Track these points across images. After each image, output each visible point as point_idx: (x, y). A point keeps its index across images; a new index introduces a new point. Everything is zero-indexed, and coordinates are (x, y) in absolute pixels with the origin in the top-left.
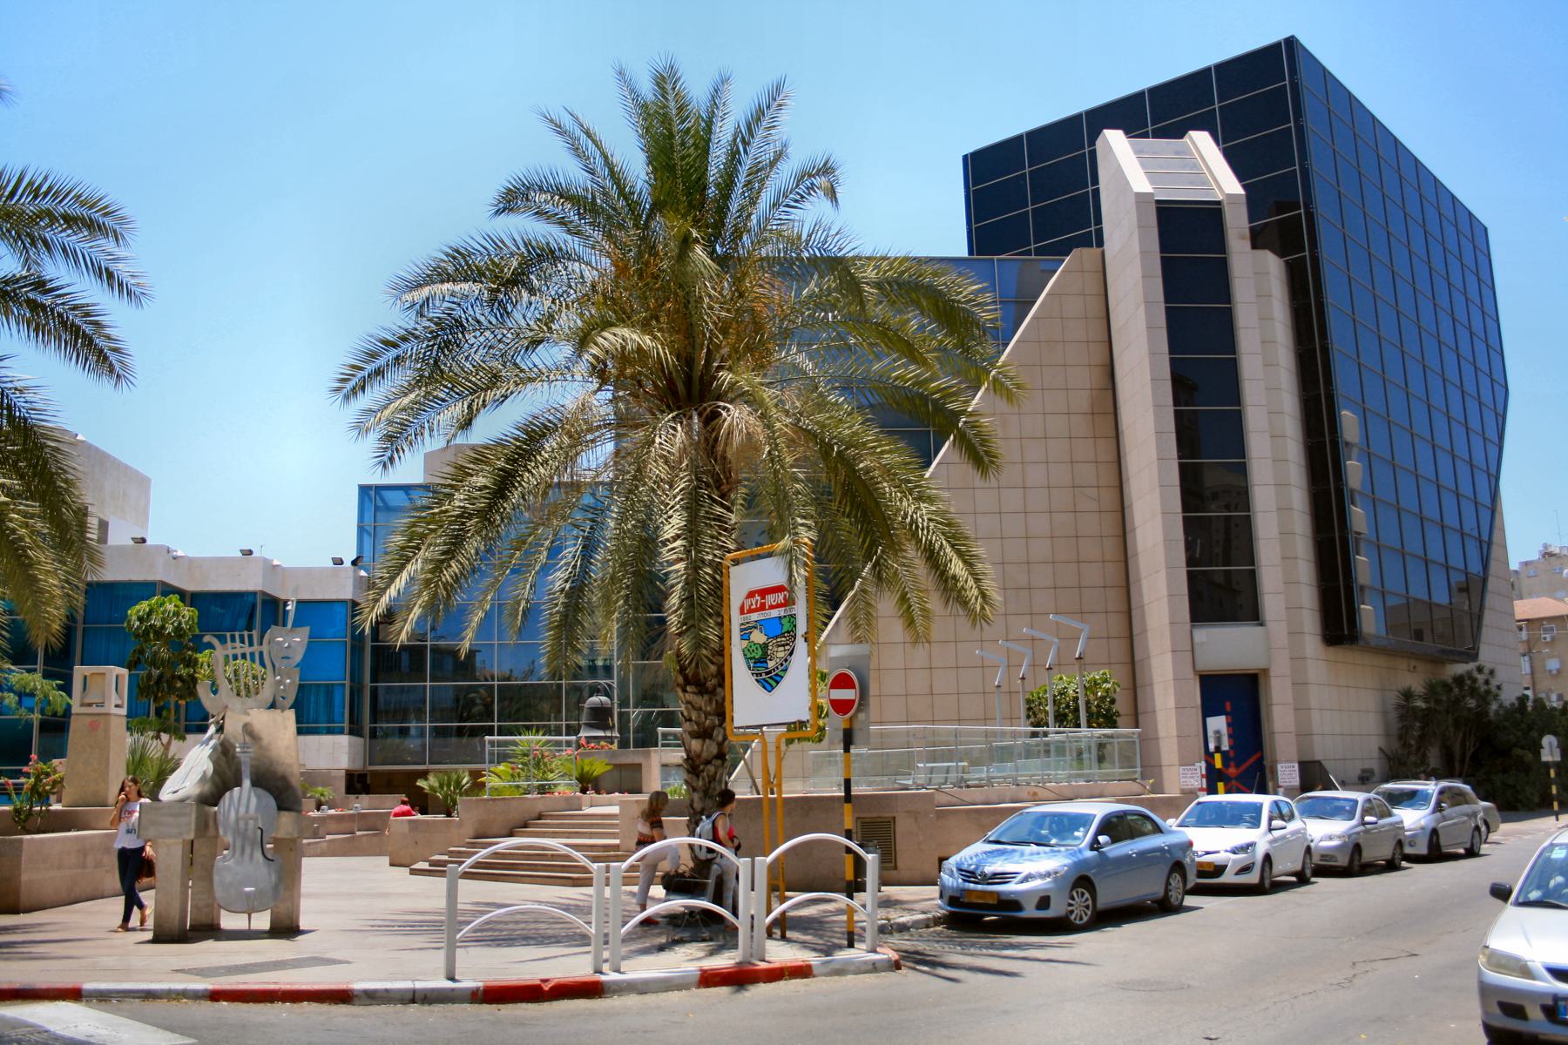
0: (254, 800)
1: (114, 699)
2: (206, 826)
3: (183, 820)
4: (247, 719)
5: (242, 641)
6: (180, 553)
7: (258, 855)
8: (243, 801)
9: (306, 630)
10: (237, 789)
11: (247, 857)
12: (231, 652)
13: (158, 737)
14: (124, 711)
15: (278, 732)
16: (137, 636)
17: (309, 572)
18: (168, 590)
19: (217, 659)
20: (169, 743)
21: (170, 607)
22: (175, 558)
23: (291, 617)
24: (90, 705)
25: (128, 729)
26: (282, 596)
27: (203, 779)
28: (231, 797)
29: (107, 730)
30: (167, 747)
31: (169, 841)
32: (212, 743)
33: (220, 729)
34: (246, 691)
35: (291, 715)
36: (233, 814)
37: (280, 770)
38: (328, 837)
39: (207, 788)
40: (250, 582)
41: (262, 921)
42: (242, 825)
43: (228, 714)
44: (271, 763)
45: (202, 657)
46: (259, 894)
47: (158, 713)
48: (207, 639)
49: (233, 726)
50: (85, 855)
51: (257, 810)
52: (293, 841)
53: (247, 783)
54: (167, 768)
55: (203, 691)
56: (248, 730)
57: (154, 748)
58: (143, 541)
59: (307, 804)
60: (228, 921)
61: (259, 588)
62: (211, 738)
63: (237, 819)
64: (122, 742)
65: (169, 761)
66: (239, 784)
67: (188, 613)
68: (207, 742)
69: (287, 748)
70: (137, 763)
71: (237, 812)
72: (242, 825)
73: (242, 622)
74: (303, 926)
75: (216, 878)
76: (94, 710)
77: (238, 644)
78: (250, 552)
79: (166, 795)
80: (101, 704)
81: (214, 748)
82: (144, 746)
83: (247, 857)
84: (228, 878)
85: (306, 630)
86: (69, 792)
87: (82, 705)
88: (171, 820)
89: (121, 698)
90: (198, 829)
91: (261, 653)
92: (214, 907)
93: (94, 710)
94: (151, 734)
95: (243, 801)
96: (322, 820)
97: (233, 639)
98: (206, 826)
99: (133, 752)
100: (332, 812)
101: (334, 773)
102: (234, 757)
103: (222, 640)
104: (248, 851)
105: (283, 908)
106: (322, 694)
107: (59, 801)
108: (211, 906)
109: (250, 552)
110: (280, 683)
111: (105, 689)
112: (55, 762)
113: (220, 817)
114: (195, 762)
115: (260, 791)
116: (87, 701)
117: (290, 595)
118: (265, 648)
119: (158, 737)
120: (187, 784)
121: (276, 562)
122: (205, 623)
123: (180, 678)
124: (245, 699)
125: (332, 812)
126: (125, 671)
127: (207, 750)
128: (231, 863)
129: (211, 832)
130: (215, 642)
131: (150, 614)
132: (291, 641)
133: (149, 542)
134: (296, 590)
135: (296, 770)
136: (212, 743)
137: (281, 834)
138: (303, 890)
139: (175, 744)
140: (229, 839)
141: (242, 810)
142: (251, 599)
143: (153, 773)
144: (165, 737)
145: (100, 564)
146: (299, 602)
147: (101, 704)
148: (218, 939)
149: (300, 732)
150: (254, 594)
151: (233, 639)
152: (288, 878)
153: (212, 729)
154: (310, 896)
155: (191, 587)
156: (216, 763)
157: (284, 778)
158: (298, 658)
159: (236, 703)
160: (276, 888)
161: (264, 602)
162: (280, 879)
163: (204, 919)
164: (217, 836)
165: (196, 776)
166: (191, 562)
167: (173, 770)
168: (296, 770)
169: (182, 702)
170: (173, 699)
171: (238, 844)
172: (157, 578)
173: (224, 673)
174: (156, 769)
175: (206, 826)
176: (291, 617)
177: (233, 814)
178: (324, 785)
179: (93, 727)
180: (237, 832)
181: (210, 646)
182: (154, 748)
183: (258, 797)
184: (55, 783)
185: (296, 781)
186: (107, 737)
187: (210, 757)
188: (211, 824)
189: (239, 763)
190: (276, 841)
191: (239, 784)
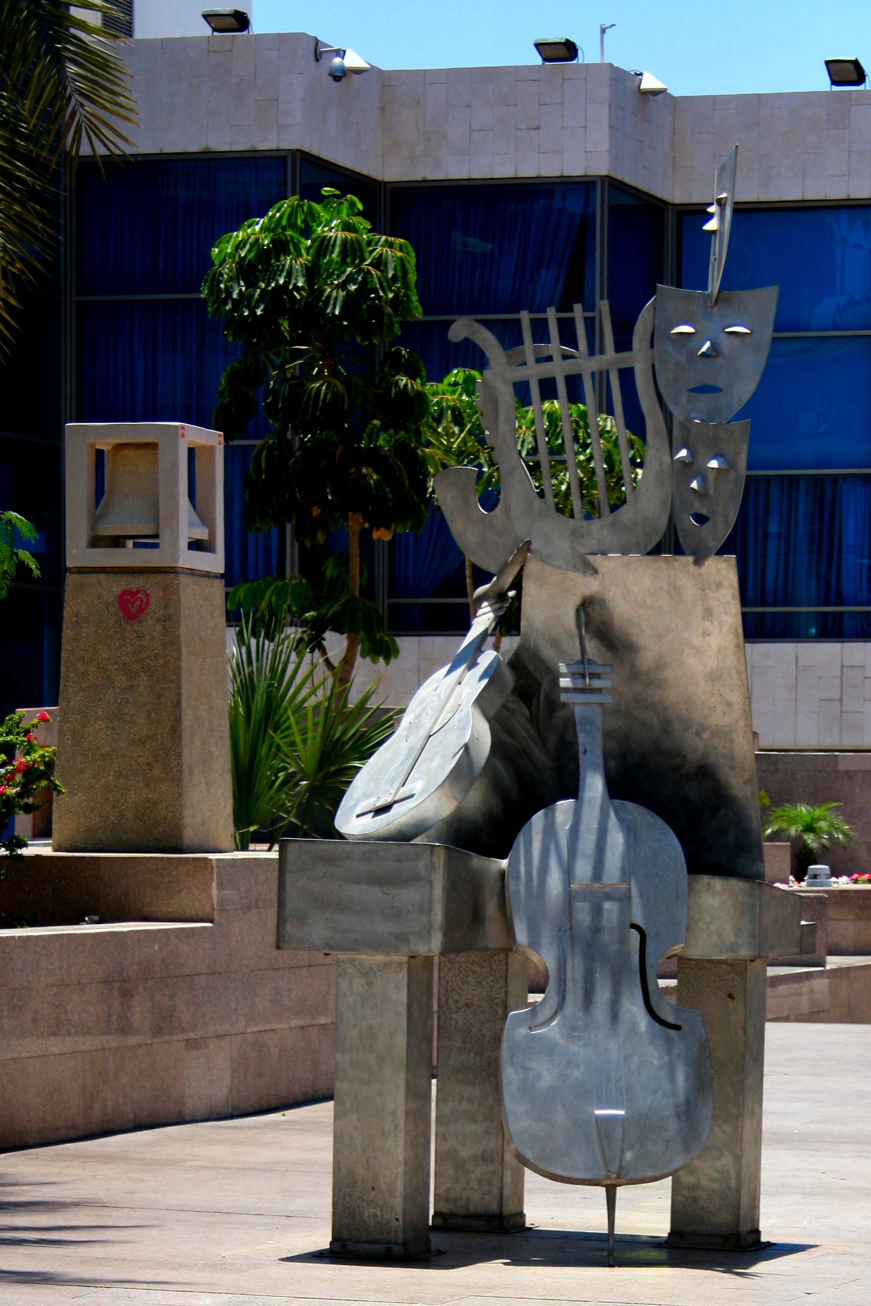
0: (617, 839)
1: (185, 525)
2: (477, 915)
3: (410, 895)
4: (590, 586)
5: (568, 337)
6: (352, 60)
7: (633, 1008)
8: (583, 839)
9: (766, 300)
10: (564, 806)
11: (600, 1012)
12: (533, 373)
13: (316, 643)
14: (215, 562)
15: (690, 627)
16: (242, 327)
17: (755, 110)
18: (311, 175)
19: (495, 406)
20: (348, 661)
21: (331, 229)
22: (340, 75)
23: (719, 253)
24: (117, 542)
25: (232, 618)
26: (676, 193)
27: (462, 772)
28: (550, 830)
29: (170, 620)
30: (342, 674)
31: (367, 959)
32: (487, 657)
33: (509, 622)
34: (599, 498)
35: (723, 572)
36: (555, 881)
37: (695, 746)
38: (833, 962)
39: (475, 798)
40: (577, 150)
41: (648, 1211)
42: (583, 913)
43: (533, 567)
44: (666, 727)
45: (445, 391)
46: (640, 1127)
47: (310, 565)
48: (461, 328)
49: (549, 605)
50: (127, 994)
51: (627, 872)
52: (739, 968)
53: (594, 785)
54: (350, 740)
55: (448, 493)
56: (592, 617)
57: (307, 678)
58: (240, 21)
59: (776, 858)
60: (550, 1206)
61: (600, 167)
62: (478, 647)
63: (569, 898)
64: (214, 655)
65: (348, 717)
66: (572, 790)
67: (392, 251)
68: (470, 658)
69: (714, 677)
70: (260, 714)
71: (568, 874)
72: (583, 913)
73: (548, 280)
74: (771, 1228)
75: (510, 1076)
76: (129, 556)
77: (555, 347)
78: (569, 50)
79: (353, 820)
80: (150, 541)
81: (493, 674)
82: (277, 674)
83: (600, 1012)
84: (546, 1075)
85: (766, 300)
86: (66, 814)
87: (96, 542)
88: (372, 894)
89: (206, 520)
90: (450, 926)
91: (627, 375)
92: (503, 1164)
93: (129, 556)
94: (292, 633)
95: (583, 839)
96: (819, 905)
97: (540, 332)
98: (474, 916)
99: (247, 689)
100: (843, 883)
101: (846, 762)
102: (553, 705)
103: (510, 337)
104: (603, 995)
105: (709, 1172)
106: (803, 504)
107: (43, 832)
108: (491, 1157)
109: (569, 50)
110: (688, 469)
111: (162, 489)
112: (27, 715)
113: (517, 889)
114: (434, 726)
115: (634, 810)
116: (108, 529)
117: (709, 186)
118: (638, 359)
119: (316, 643)
120: (416, 785)
121: (649, 82)
122: (446, 284)
123: (374, 457)
124: (578, 521)
125: (843, 883)
126: (210, 438)
127: (472, 683)
128: (552, 1030)
129: (493, 934)
130: (487, 340)
131: (280, 247)
132: (718, 334)
133: (258, 26)
134: (729, 171)
135: (744, 748)
136: (487, 657)
137: (702, 947)
138: (768, 1123)
139: (365, 671)
140: (546, 958)
141: (583, 869)
142: (574, 206)
143: (307, 752)
144: (336, 644)
145: (125, 113)
146: (745, 213)
147: (150, 541)
148: (519, 1260)
149: (756, 629)
150: (585, 186)
151: (540, 332)
152: (724, 1080)
153: (484, 619)
154: (787, 1140)
155: (391, 170)
156: (498, 723)
157: (705, 772)
158: (745, 387)
159: (553, 535)
160: (688, 1113)
161: (615, 212)
162: (701, 1083)
163: (478, 1198)
164: (509, 947)
165: (440, 762)
166: (387, 90)
167: (365, 748)
168: (744, 748)
169: (382, 535)
170: (355, 524)
171: (576, 969)
172: (290, 141)
173: (520, 431)
174: (314, 738)
175: (474, 916)
176: (719, 253)
177: (555, 881)
178: (815, 800)
179: (131, 607)
180: (567, 933)
181: (474, 358)
182: (307, 678)
183: (629, 830)
184: (30, 774)
185: (741, 783)
186: (172, 642)
187: (481, 702)
188: (491, 909)
189: (570, 722)
190: (685, 968)
191: (572, 790)
